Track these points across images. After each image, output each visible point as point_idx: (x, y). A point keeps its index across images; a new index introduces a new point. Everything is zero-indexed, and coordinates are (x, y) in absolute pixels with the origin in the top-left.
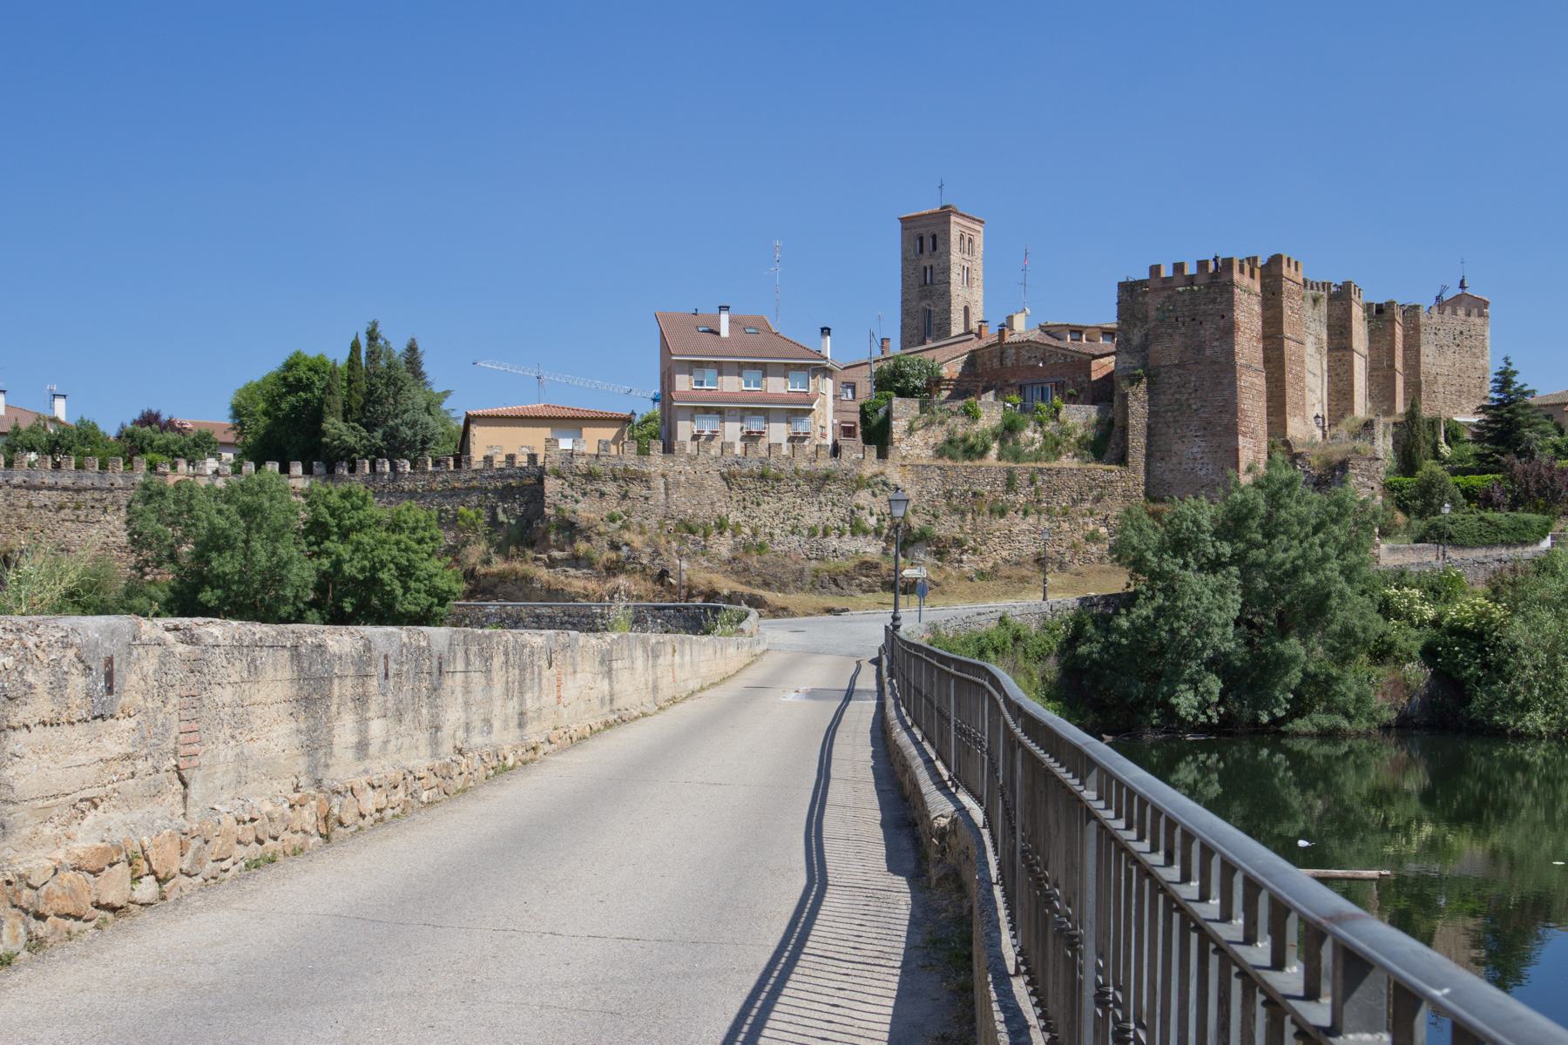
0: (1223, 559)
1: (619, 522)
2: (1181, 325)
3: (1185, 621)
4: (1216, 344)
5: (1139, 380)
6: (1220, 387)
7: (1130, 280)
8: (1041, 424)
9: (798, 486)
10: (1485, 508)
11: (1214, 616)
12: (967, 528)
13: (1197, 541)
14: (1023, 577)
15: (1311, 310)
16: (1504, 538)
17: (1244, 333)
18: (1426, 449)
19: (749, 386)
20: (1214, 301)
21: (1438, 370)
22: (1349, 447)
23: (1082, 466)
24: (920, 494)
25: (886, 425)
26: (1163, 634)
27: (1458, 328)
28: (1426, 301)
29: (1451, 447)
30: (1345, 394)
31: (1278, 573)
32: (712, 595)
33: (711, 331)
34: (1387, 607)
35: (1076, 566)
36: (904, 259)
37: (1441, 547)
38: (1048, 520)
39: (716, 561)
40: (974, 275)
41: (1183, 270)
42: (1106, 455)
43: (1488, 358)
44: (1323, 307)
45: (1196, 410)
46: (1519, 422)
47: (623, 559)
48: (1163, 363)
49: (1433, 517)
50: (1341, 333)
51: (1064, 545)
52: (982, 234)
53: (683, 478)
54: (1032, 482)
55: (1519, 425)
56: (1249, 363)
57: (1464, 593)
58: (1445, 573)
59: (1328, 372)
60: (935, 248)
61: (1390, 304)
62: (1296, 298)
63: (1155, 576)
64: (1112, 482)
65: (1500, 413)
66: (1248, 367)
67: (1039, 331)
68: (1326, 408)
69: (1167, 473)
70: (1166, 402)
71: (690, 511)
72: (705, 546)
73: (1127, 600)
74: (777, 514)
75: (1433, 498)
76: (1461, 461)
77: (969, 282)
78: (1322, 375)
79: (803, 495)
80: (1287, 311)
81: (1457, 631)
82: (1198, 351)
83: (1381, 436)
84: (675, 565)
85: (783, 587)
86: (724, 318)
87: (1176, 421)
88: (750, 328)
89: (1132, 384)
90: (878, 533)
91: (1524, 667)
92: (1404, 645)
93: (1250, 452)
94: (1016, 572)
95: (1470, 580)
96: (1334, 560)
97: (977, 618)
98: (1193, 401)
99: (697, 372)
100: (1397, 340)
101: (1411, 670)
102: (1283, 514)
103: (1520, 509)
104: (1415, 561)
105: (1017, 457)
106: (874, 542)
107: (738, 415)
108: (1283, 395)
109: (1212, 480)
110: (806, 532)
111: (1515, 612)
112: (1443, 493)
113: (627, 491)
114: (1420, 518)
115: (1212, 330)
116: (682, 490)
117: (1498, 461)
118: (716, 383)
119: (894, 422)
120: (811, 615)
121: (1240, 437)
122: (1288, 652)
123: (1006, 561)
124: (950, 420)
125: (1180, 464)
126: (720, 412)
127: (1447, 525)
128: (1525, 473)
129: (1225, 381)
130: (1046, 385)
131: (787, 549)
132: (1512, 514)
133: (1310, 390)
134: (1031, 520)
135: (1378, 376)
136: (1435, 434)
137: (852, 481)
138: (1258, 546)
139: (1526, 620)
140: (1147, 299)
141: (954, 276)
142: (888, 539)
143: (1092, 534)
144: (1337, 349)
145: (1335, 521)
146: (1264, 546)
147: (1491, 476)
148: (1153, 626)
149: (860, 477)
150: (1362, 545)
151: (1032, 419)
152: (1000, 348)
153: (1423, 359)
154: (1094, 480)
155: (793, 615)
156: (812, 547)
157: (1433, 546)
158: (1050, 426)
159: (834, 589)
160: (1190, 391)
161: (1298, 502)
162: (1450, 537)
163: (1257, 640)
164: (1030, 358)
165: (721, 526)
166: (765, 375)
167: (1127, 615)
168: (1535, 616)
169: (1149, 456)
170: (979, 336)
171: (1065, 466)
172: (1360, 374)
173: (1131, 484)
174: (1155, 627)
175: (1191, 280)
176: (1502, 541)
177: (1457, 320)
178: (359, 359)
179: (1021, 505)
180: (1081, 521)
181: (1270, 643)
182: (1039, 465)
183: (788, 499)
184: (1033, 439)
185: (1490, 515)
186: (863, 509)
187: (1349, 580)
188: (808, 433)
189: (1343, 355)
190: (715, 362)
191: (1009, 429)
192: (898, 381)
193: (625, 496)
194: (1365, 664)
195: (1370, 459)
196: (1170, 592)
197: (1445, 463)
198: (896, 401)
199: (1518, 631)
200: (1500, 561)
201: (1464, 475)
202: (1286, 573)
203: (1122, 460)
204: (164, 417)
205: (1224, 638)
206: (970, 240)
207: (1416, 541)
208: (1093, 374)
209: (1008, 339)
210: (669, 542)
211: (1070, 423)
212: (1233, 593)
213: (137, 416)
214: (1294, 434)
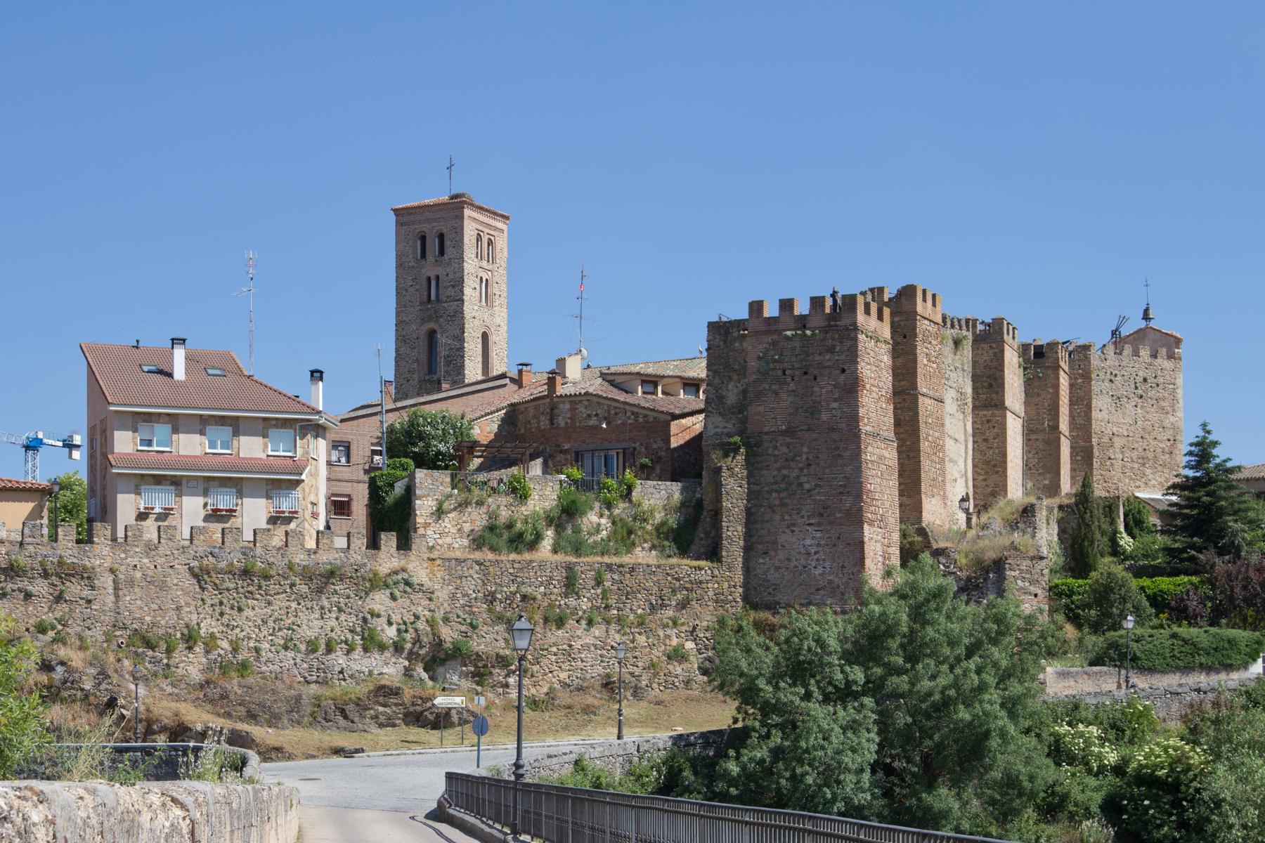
0: (854, 688)
1: (51, 634)
2: (789, 380)
3: (810, 765)
4: (835, 405)
5: (736, 451)
6: (840, 461)
7: (724, 319)
8: (609, 505)
9: (292, 585)
10: (1178, 621)
11: (846, 760)
13: (822, 665)
14: (588, 706)
15: (951, 356)
16: (1203, 660)
17: (870, 391)
18: (1102, 542)
19: (215, 448)
20: (831, 350)
21: (1115, 429)
22: (1006, 541)
23: (663, 562)
24: (453, 597)
25: (406, 505)
26: (783, 782)
27: (1141, 374)
28: (1099, 337)
29: (1134, 537)
30: (995, 466)
31: (924, 706)
32: (179, 731)
33: (161, 372)
34: (1058, 749)
35: (656, 692)
36: (400, 265)
37: (1123, 672)
38: (619, 632)
39: (183, 686)
40: (495, 289)
41: (792, 308)
42: (693, 547)
43: (1180, 414)
44: (967, 350)
45: (809, 491)
46: (1221, 508)
47: (57, 683)
48: (766, 429)
49: (1112, 633)
50: (991, 385)
51: (640, 664)
52: (506, 235)
53: (138, 575)
54: (599, 582)
55: (1221, 512)
56: (876, 430)
57: (1154, 731)
58: (1129, 706)
59: (974, 436)
60: (442, 252)
61: (1053, 346)
62: (934, 342)
63: (767, 709)
64: (701, 582)
65: (1196, 495)
66: (876, 435)
67: (600, 380)
68: (970, 484)
69: (772, 571)
70: (770, 479)
71: (148, 619)
72: (168, 665)
73: (736, 738)
74: (265, 622)
75: (1112, 607)
76: (1146, 556)
77: (488, 299)
78: (966, 441)
79: (300, 598)
80: (922, 360)
81: (1146, 779)
82: (812, 413)
83: (1044, 525)
84: (129, 691)
85: (273, 720)
86: (179, 354)
87: (783, 505)
88: (213, 368)
89: (726, 455)
90: (398, 648)
91: (1231, 827)
92: (1080, 798)
93: (879, 545)
94: (578, 700)
95: (1161, 715)
96: (992, 690)
97: (547, 762)
98: (804, 479)
99: (143, 427)
100: (1062, 393)
101: (1089, 829)
102: (930, 632)
103: (1224, 621)
104: (1091, 690)
105: (577, 549)
106: (394, 660)
107: (201, 488)
108: (916, 469)
109: (831, 582)
110: (303, 647)
111: (1218, 756)
112: (1124, 600)
113: (62, 592)
114: (1095, 632)
115: (830, 388)
116: (137, 590)
117: (1192, 559)
118: (170, 443)
119: (418, 502)
120: (313, 757)
121: (866, 526)
122: (938, 805)
123: (565, 685)
124: (490, 500)
125: (789, 560)
126: (176, 482)
127: (1130, 643)
128: (1229, 575)
129: (847, 454)
130: (611, 453)
131: (279, 670)
132: (1213, 630)
133: (951, 461)
134: (597, 631)
135: (1037, 440)
136: (1113, 522)
137: (364, 579)
138: (899, 672)
139: (1233, 767)
140: (745, 345)
141: (468, 291)
142: (412, 656)
143: (676, 650)
144: (985, 406)
145: (995, 642)
146: (906, 672)
147: (1186, 579)
148: (769, 772)
149: (375, 575)
150: (1028, 671)
151: (597, 499)
152: (549, 402)
153: (1095, 414)
154: (678, 579)
155: (290, 757)
156: (310, 669)
157: (1114, 670)
158: (621, 508)
159: (342, 722)
160: (801, 465)
161: (948, 617)
162: (1135, 659)
163: (898, 790)
164: (589, 416)
165: (190, 639)
166: (236, 433)
167: (737, 758)
168: (1243, 763)
169: (748, 549)
170: (518, 382)
171: (640, 561)
172: (1015, 439)
173: (726, 585)
174: (772, 773)
175: (802, 321)
176: (1201, 664)
177: (1140, 363)
179: (585, 612)
180: (661, 633)
181: (915, 794)
182: (607, 559)
183: (280, 602)
184: (599, 525)
185: (1184, 630)
186: (379, 616)
187: (1013, 715)
188: (296, 512)
189: (993, 415)
190: (169, 415)
191: (568, 513)
192: (415, 445)
193: (59, 598)
194: (1031, 822)
195: (1032, 558)
196: (791, 727)
197: (1126, 559)
198: (420, 474)
199: (1223, 782)
200: (1198, 690)
201: (1151, 576)
202: (934, 705)
203: (713, 554)
205: (858, 788)
206: (490, 242)
207: (1091, 664)
208: (672, 439)
209: (560, 390)
210: (119, 660)
211: (646, 505)
212: (868, 731)
214: (932, 520)
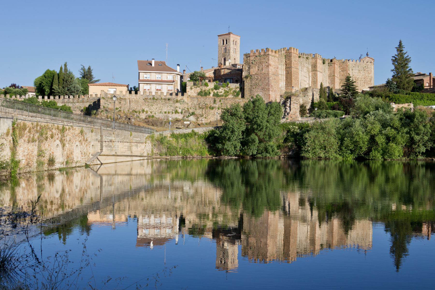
12: (204, 113)
53: (134, 100)
78: (309, 78)
144: (313, 71)
178: (62, 71)
204: (17, 85)
213: (10, 85)
